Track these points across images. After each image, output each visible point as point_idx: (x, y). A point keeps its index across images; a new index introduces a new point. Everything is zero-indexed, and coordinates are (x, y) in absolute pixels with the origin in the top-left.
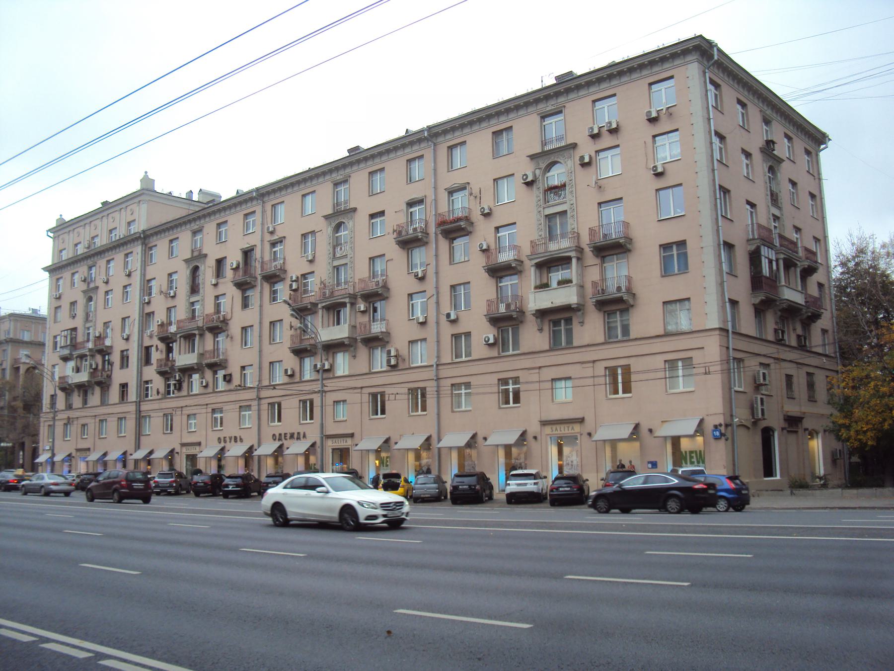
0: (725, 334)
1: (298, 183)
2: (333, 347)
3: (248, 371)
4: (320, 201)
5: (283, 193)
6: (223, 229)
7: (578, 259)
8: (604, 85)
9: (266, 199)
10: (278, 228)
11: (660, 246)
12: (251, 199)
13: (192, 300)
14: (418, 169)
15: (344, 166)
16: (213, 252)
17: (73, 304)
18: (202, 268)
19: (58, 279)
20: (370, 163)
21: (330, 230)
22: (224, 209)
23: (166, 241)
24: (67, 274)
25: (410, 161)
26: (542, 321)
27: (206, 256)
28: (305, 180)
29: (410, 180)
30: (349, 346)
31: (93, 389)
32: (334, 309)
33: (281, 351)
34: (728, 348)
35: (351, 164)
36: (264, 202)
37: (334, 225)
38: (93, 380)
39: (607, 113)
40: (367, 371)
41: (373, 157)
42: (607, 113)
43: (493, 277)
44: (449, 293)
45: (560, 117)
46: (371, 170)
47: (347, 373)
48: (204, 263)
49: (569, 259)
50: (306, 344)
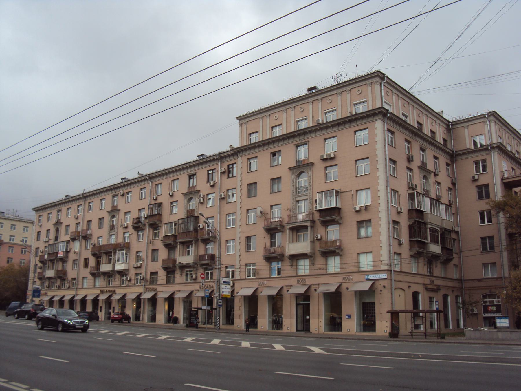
0: (389, 272)
1: (99, 193)
2: (295, 258)
3: (85, 280)
4: (181, 185)
5: (178, 173)
6: (103, 202)
7: (312, 227)
8: (329, 130)
9: (224, 160)
10: (159, 198)
11: (357, 222)
12: (81, 198)
13: (111, 234)
14: (254, 165)
15: (194, 166)
16: (65, 221)
17: (48, 231)
18: (60, 229)
19: (40, 216)
20: (208, 164)
21: (186, 201)
22: (130, 184)
23: (245, 159)
24: (45, 214)
25: (173, 181)
26: (292, 261)
27: (119, 210)
28: (101, 192)
29: (249, 171)
30: (311, 257)
31: (115, 276)
32: (298, 230)
33: (257, 257)
34: (391, 280)
35: (198, 165)
36: (85, 201)
37: (188, 198)
38: (199, 262)
39: (332, 147)
40: (268, 276)
41: (210, 161)
42: (332, 147)
43: (268, 233)
44: (356, 226)
45: (306, 147)
46: (101, 198)
47: (338, 270)
48: (119, 213)
49: (306, 227)
50: (41, 277)
